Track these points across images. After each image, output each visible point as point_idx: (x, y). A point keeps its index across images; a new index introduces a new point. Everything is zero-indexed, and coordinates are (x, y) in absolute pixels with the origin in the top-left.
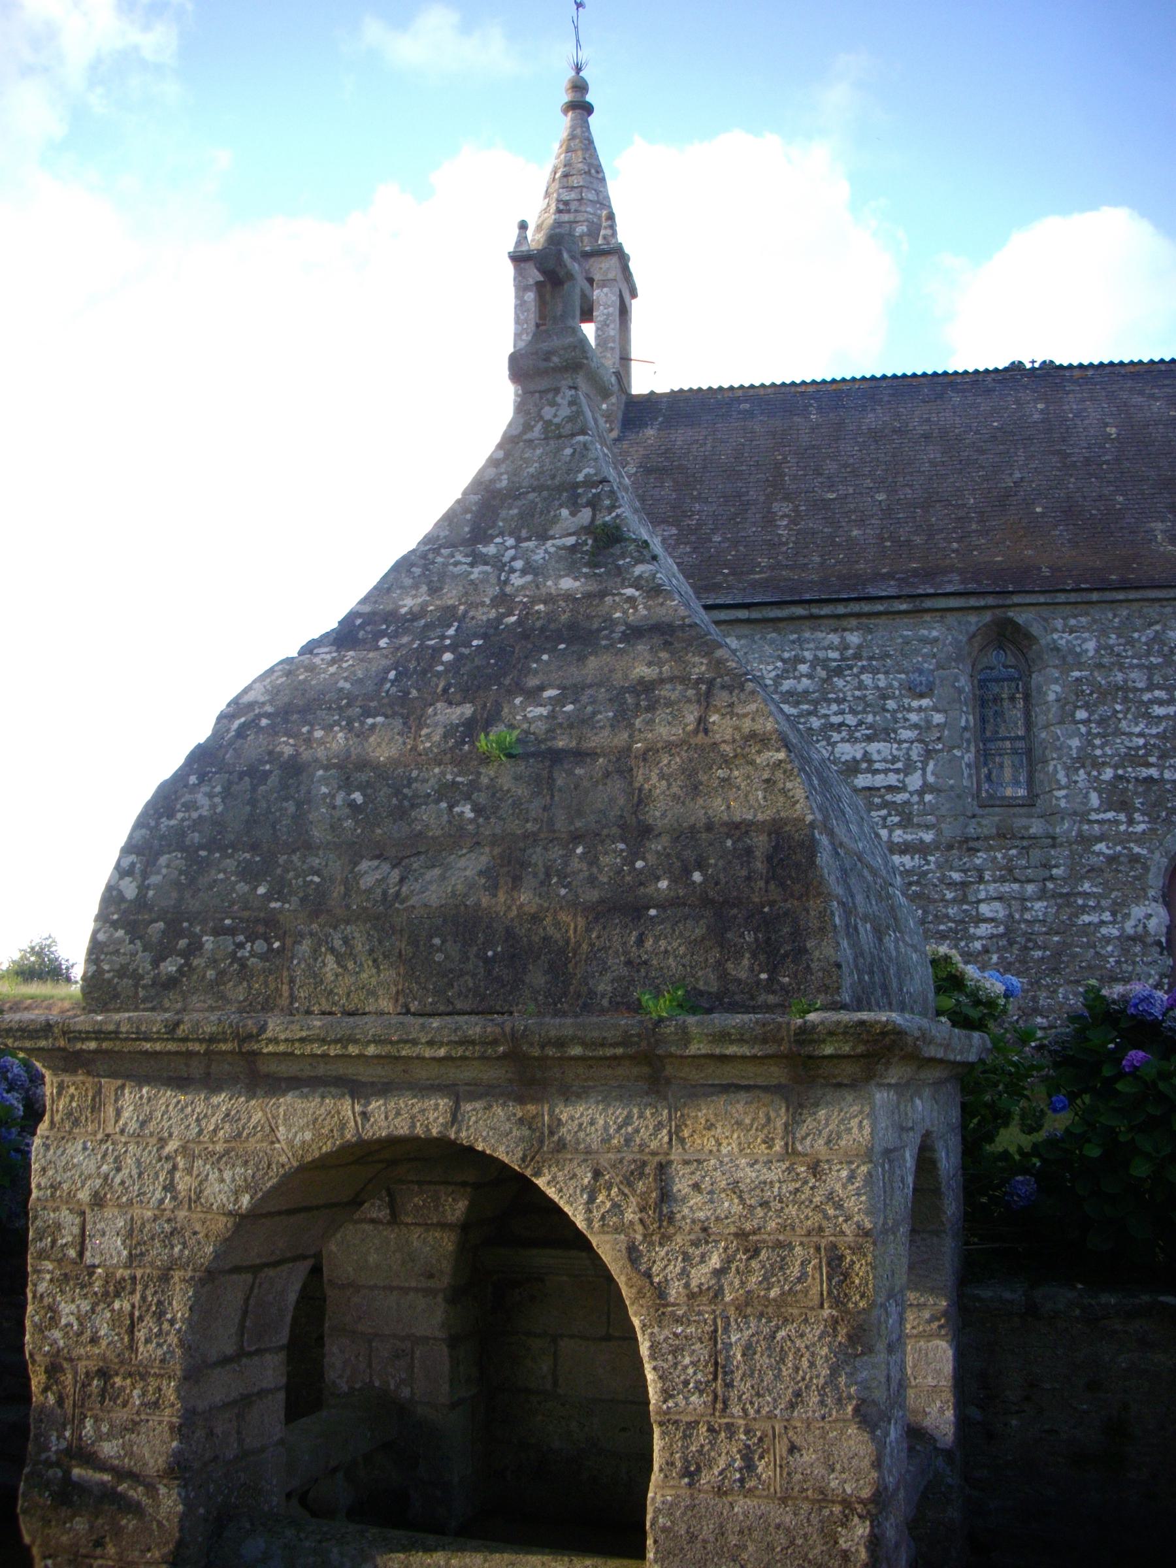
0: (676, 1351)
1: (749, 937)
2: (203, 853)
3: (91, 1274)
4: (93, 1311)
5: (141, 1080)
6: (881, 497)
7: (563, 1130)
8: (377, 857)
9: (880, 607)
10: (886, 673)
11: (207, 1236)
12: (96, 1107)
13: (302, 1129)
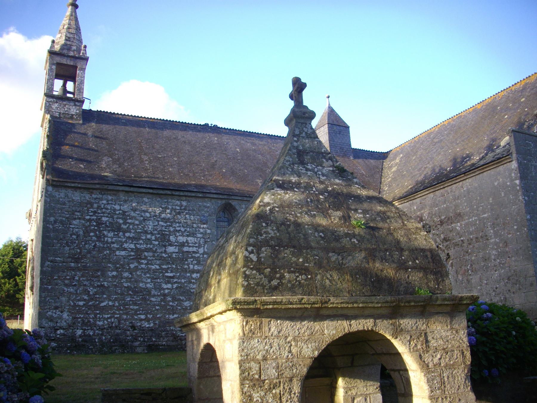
0: (433, 380)
1: (432, 277)
2: (277, 248)
3: (264, 383)
4: (265, 394)
5: (277, 318)
6: (176, 159)
7: (402, 326)
8: (334, 252)
9: (193, 194)
10: (194, 215)
11: (304, 365)
12: (260, 328)
13: (332, 330)
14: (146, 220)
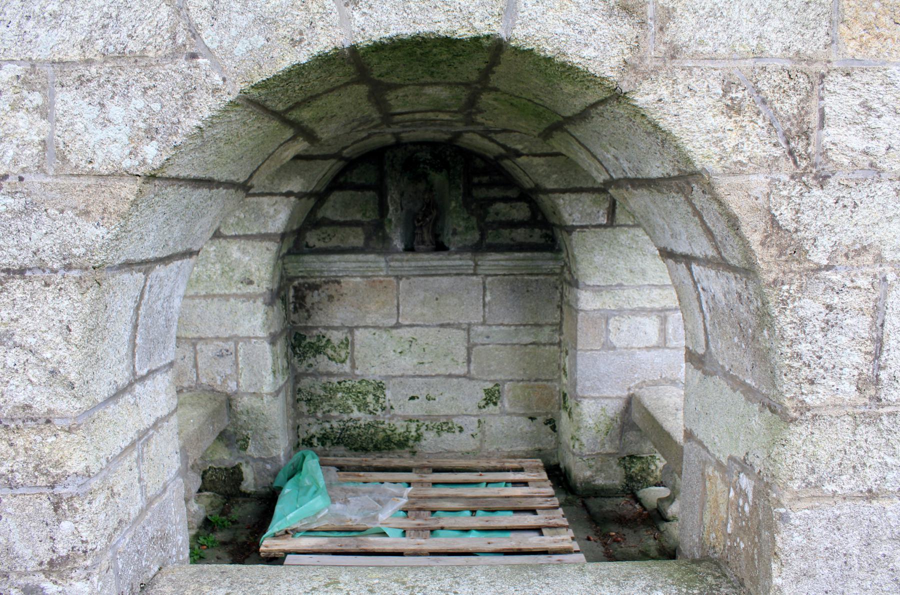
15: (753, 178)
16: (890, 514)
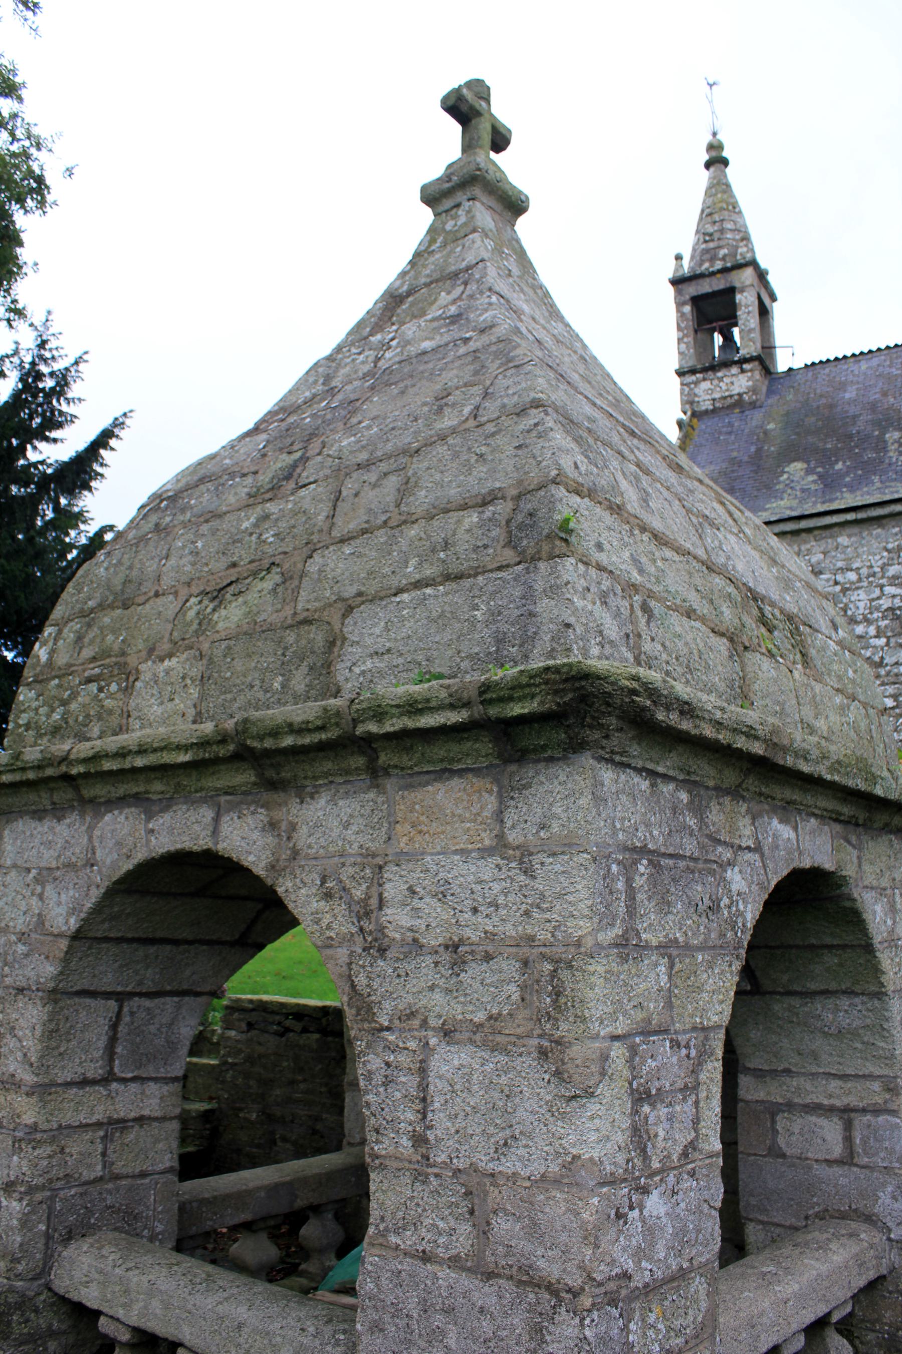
14: (848, 589)
15: (339, 950)
16: (441, 1281)
